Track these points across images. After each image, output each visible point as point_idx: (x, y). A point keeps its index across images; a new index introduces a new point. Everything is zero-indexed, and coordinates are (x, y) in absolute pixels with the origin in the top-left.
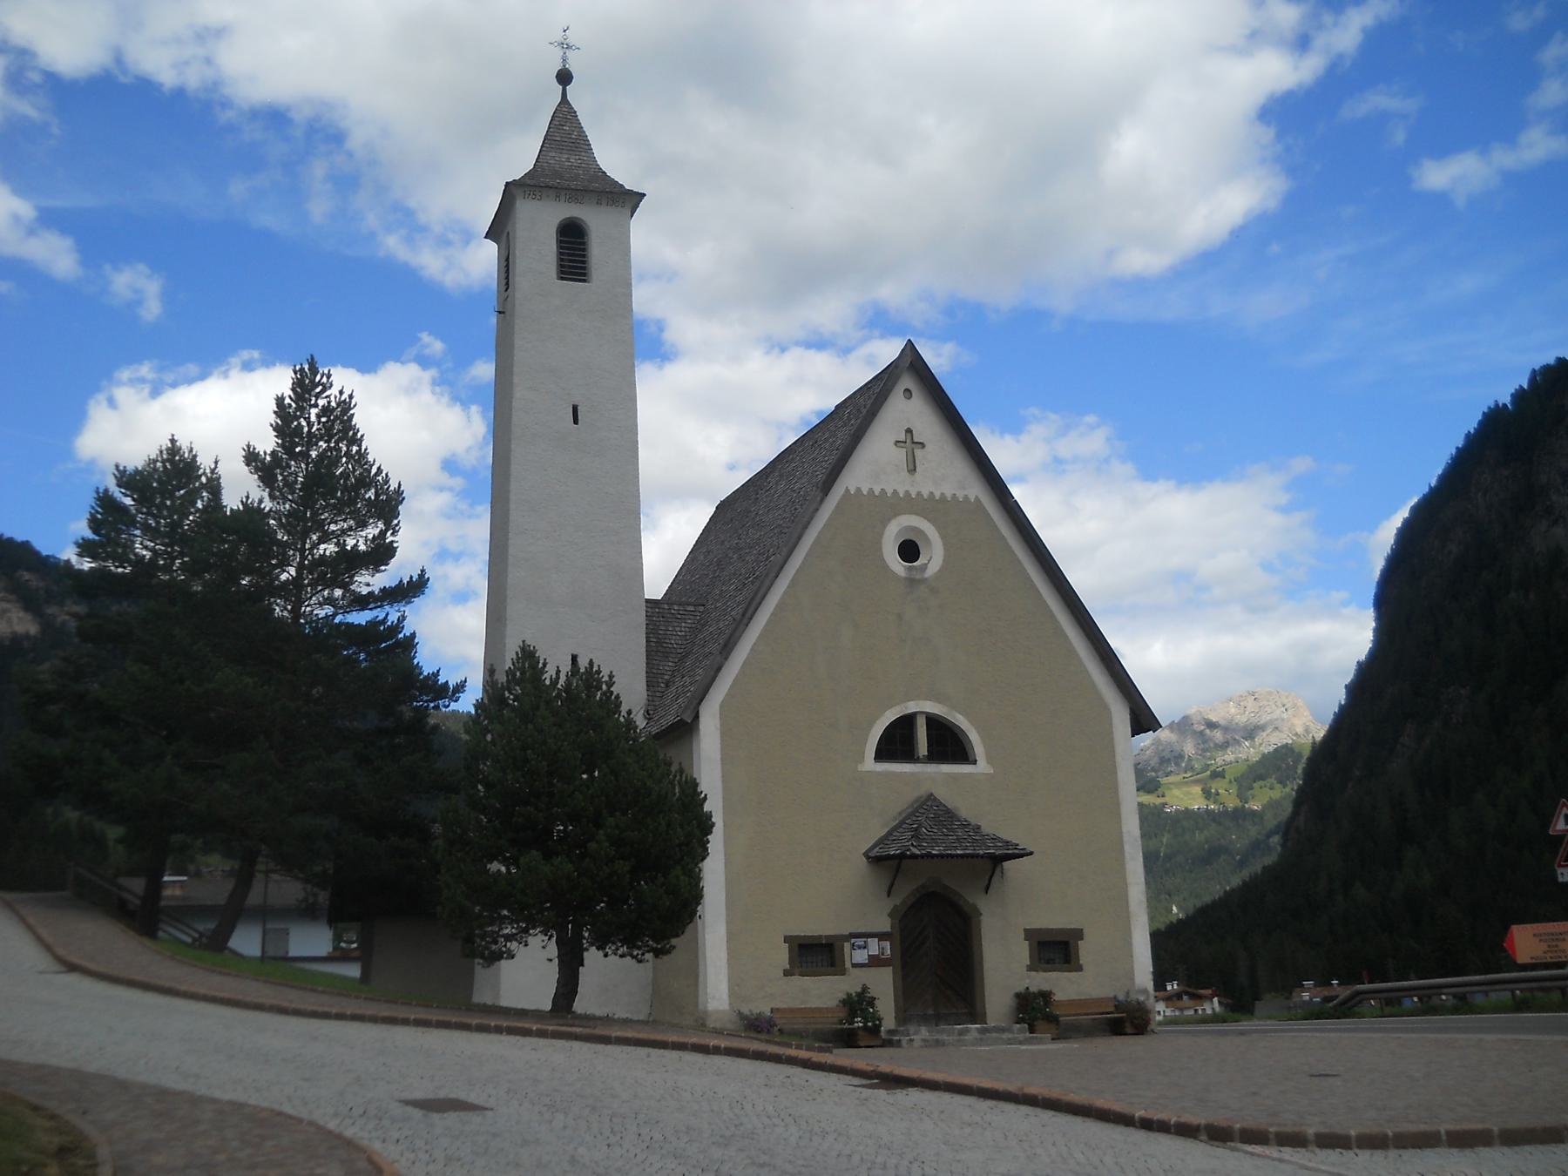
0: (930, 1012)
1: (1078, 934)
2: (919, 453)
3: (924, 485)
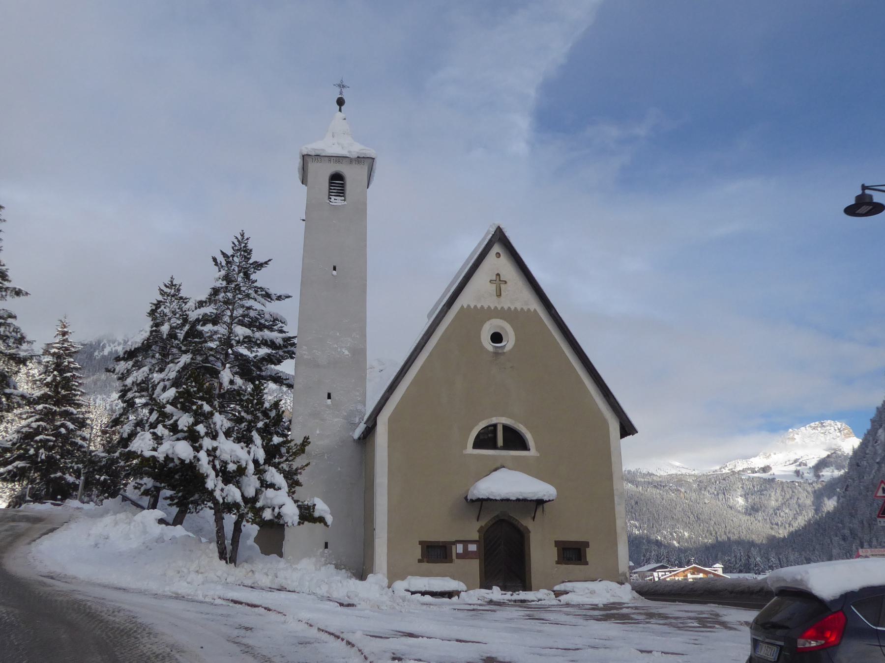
1: (558, 563)
3: (505, 303)
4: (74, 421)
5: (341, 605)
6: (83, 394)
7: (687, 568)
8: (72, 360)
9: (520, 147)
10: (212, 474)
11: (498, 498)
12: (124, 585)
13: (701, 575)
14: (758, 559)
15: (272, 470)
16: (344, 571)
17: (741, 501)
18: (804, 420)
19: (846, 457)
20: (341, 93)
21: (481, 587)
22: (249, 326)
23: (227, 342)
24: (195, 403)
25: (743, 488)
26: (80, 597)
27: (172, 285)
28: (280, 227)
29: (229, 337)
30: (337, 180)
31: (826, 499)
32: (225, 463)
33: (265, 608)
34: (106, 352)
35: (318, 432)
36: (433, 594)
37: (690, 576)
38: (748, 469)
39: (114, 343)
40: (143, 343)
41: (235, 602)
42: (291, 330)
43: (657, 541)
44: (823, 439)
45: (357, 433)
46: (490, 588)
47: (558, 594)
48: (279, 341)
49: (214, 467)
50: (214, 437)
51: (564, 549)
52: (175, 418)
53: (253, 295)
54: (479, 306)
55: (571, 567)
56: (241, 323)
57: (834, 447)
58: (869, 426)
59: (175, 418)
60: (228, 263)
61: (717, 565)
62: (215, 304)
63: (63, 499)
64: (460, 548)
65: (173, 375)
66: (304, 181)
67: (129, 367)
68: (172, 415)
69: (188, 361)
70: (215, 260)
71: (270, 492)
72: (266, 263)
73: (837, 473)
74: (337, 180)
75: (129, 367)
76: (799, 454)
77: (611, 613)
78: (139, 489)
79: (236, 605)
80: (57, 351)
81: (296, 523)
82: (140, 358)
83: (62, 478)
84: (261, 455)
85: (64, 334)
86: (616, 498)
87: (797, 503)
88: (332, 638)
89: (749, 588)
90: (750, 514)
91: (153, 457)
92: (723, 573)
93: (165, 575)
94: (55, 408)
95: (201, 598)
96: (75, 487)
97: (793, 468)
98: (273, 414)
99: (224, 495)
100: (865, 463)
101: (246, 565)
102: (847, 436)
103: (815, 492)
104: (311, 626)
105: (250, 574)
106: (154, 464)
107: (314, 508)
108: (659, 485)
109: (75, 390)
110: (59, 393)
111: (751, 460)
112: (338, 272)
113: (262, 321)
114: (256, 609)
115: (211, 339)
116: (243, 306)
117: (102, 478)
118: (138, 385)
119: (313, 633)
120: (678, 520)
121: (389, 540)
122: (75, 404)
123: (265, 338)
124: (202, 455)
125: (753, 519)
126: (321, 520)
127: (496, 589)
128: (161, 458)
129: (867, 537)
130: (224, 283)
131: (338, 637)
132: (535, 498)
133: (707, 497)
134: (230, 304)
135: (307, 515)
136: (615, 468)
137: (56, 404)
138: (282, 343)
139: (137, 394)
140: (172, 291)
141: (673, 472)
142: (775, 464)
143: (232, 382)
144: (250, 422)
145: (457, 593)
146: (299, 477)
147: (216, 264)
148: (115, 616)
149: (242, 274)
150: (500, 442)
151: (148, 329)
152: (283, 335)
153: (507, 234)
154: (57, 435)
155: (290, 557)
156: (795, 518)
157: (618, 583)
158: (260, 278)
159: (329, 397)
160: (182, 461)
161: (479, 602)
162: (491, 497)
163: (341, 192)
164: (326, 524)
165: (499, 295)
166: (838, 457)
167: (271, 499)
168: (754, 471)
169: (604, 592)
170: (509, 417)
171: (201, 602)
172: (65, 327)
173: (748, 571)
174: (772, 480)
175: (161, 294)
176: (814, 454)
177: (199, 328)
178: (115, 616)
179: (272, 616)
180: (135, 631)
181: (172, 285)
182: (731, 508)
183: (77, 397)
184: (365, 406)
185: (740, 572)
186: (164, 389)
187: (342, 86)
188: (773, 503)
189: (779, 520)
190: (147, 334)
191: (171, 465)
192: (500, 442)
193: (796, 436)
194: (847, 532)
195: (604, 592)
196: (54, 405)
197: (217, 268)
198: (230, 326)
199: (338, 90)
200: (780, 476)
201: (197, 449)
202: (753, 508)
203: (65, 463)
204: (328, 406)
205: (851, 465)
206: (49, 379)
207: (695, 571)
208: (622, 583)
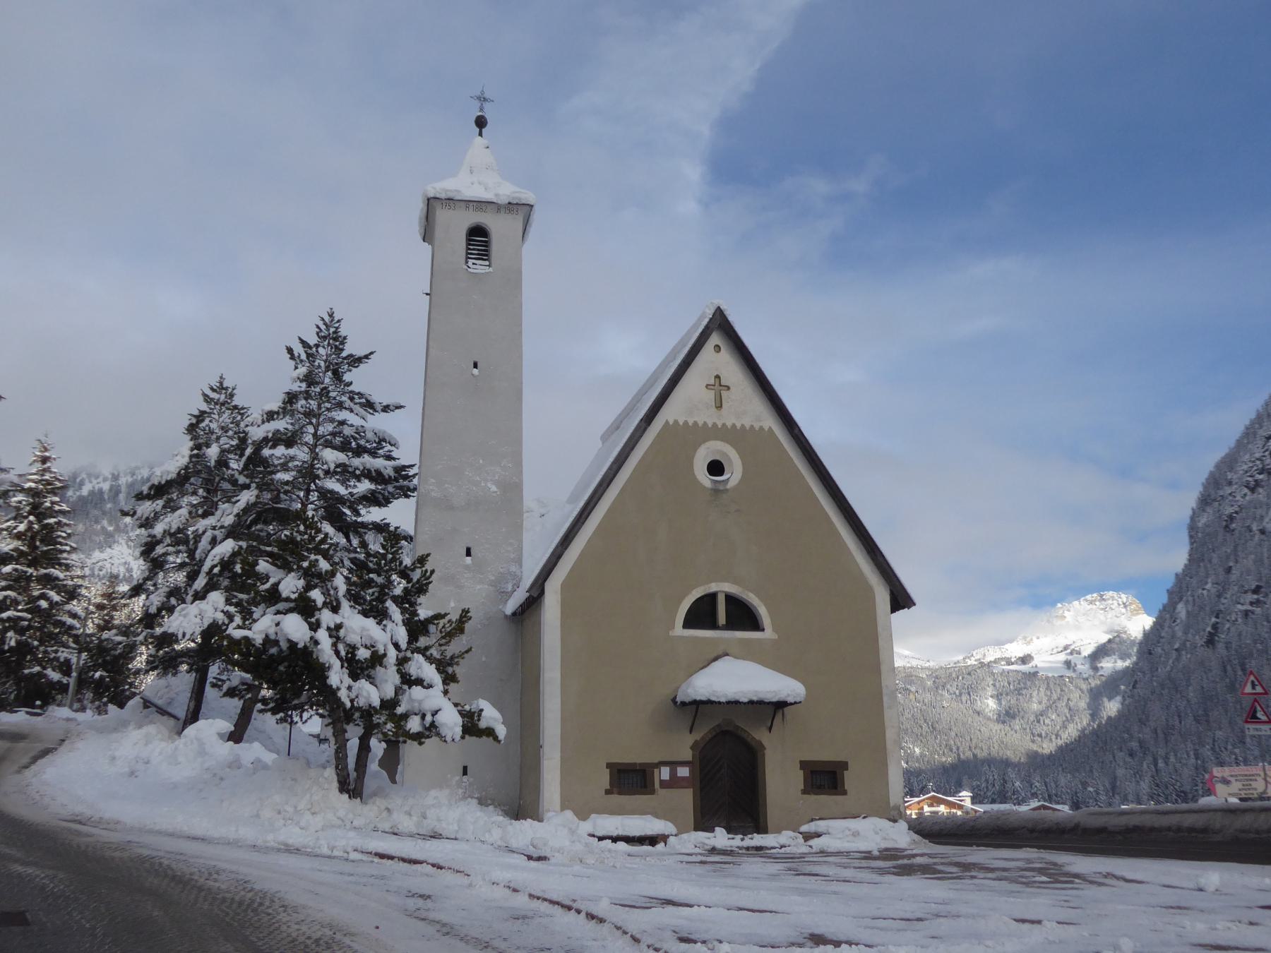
1: (804, 792)
3: (728, 418)
4: (60, 589)
5: (530, 858)
6: (74, 550)
7: (923, 797)
8: (57, 499)
9: (689, 207)
10: (336, 664)
11: (723, 700)
12: (199, 832)
13: (942, 809)
14: (1018, 784)
15: (419, 658)
16: (491, 808)
17: (992, 704)
19: (1133, 642)
20: (481, 110)
21: (696, 829)
22: (344, 447)
23: (308, 473)
24: (304, 559)
25: (994, 685)
26: (145, 852)
27: (221, 388)
28: (388, 303)
29: (312, 466)
30: (478, 238)
31: (1105, 699)
32: (352, 649)
33: (433, 865)
34: (85, 491)
36: (629, 840)
37: (927, 809)
38: (1002, 659)
39: (97, 477)
40: (179, 474)
41: (382, 856)
42: (407, 454)
44: (1102, 618)
45: (511, 606)
46: (710, 829)
47: (808, 837)
48: (389, 472)
49: (337, 653)
50: (335, 609)
52: (272, 581)
53: (348, 403)
55: (823, 798)
56: (329, 444)
57: (1117, 628)
58: (1164, 599)
59: (272, 581)
60: (308, 355)
61: (964, 793)
62: (292, 415)
63: (46, 703)
64: (665, 773)
65: (229, 520)
66: (427, 236)
67: (159, 508)
68: (267, 577)
69: (253, 499)
70: (290, 351)
71: (417, 691)
72: (367, 357)
73: (1121, 665)
74: (478, 238)
75: (159, 508)
76: (1069, 637)
77: (896, 863)
78: (219, 687)
79: (385, 861)
80: (33, 485)
81: (458, 738)
82: (174, 496)
83: (40, 675)
84: (402, 635)
85: (44, 460)
86: (885, 699)
88: (557, 910)
90: (1004, 722)
91: (246, 639)
92: (973, 803)
93: (258, 816)
94: (30, 571)
95: (325, 851)
96: (63, 688)
97: (1062, 657)
98: (416, 575)
99: (353, 695)
100: (1159, 650)
101: (378, 801)
102: (1135, 613)
103: (1091, 690)
104: (515, 890)
105: (385, 814)
106: (248, 649)
107: (480, 715)
109: (61, 544)
110: (37, 548)
111: (1007, 646)
112: (479, 370)
113: (362, 442)
114: (418, 866)
115: (285, 467)
116: (332, 420)
117: (97, 675)
118: (171, 535)
119: (521, 901)
121: (564, 760)
122: (60, 565)
123: (368, 466)
124: (322, 635)
125: (1007, 728)
126: (490, 732)
127: (720, 831)
128: (258, 640)
129: (1162, 752)
130: (304, 385)
131: (569, 908)
132: (774, 700)
133: (946, 699)
134: (314, 416)
135: (472, 726)
137: (33, 563)
138: (392, 474)
139: (171, 549)
140: (222, 397)
142: (1039, 653)
144: (382, 587)
145: (664, 838)
146: (459, 670)
147: (292, 357)
148: (215, 880)
149: (329, 373)
150: (722, 618)
151: (187, 453)
152: (392, 463)
153: (730, 319)
154: (35, 611)
156: (1064, 727)
157: (890, 820)
158: (357, 379)
159: (468, 553)
160: (292, 645)
161: (697, 850)
162: (713, 699)
163: (484, 254)
164: (496, 738)
165: (719, 406)
166: (1122, 642)
167: (420, 702)
168: (1009, 663)
169: (872, 833)
171: (329, 857)
172: (46, 450)
174: (1033, 675)
175: (206, 401)
176: (1089, 637)
177: (266, 452)
178: (215, 880)
179: (447, 877)
180: (261, 904)
181: (221, 388)
182: (979, 713)
183: (65, 555)
184: (521, 566)
185: (993, 802)
186: (214, 542)
187: (482, 99)
188: (1035, 706)
190: (185, 460)
191: (273, 651)
192: (722, 618)
193: (1066, 614)
194: (1134, 744)
195: (872, 833)
196: (29, 566)
197: (293, 363)
198: (312, 449)
199: (477, 104)
201: (315, 627)
202: (1007, 713)
203: (45, 652)
204: (467, 567)
205: (1140, 653)
206: (22, 527)
207: (935, 801)
208: (895, 821)
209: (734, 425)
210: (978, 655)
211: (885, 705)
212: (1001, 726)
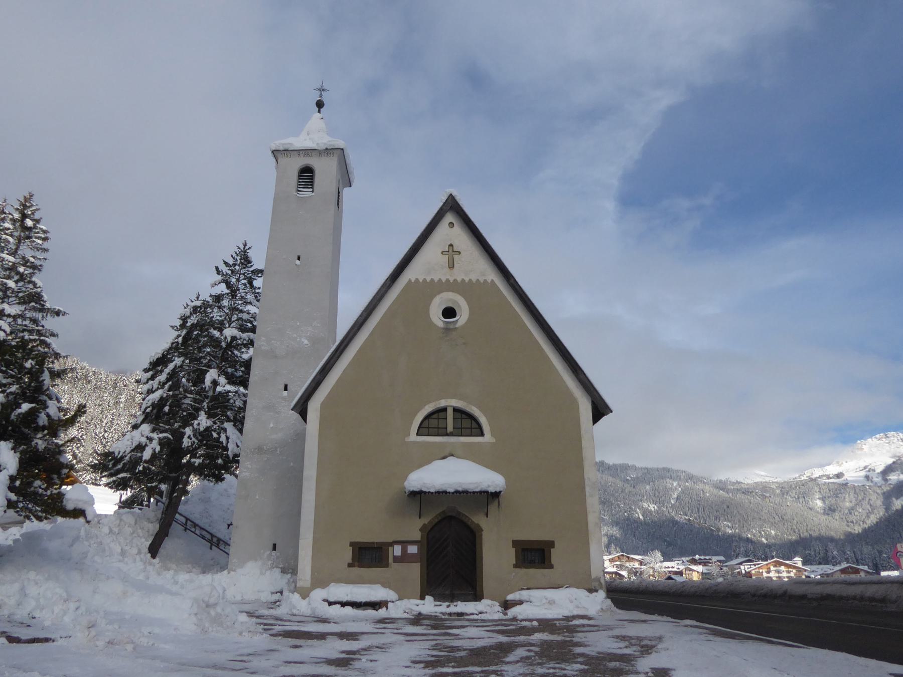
0: (447, 593)
1: (516, 566)
2: (456, 257)
3: (458, 275)
11: (432, 490)
14: (835, 552)
17: (819, 503)
18: (872, 433)
20: (321, 96)
30: (307, 175)
35: (271, 425)
38: (824, 476)
43: (748, 538)
51: (523, 550)
54: (428, 280)
64: (397, 550)
70: (217, 268)
74: (307, 175)
86: (587, 489)
87: (869, 503)
89: (771, 590)
97: (863, 473)
103: (884, 494)
108: (747, 491)
120: (765, 521)
125: (830, 518)
132: (478, 490)
136: (586, 453)
141: (758, 480)
143: (215, 383)
155: (235, 560)
156: (868, 517)
159: (286, 388)
162: (424, 490)
165: (451, 266)
168: (828, 477)
170: (461, 398)
173: (827, 563)
174: (845, 485)
176: (881, 461)
188: (848, 504)
189: (851, 518)
193: (864, 447)
200: (851, 481)
202: (830, 509)
204: (284, 399)
208: (591, 591)
209: (463, 280)
210: (808, 473)
211: (587, 494)
212: (826, 517)
